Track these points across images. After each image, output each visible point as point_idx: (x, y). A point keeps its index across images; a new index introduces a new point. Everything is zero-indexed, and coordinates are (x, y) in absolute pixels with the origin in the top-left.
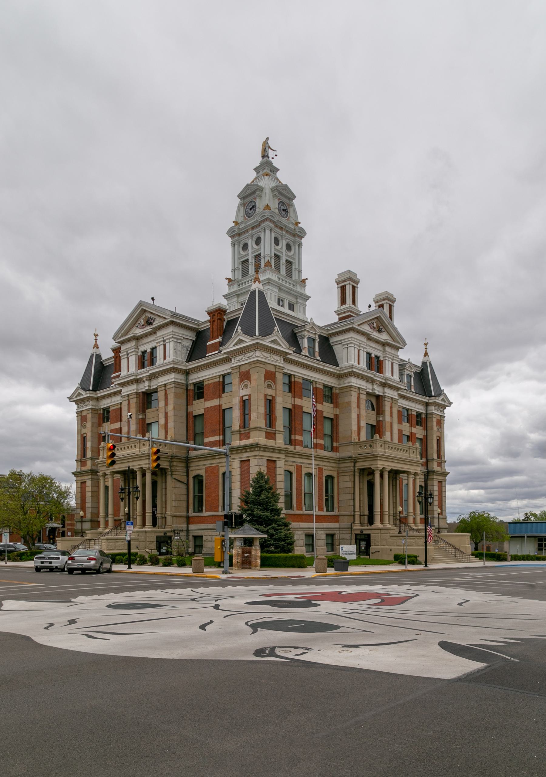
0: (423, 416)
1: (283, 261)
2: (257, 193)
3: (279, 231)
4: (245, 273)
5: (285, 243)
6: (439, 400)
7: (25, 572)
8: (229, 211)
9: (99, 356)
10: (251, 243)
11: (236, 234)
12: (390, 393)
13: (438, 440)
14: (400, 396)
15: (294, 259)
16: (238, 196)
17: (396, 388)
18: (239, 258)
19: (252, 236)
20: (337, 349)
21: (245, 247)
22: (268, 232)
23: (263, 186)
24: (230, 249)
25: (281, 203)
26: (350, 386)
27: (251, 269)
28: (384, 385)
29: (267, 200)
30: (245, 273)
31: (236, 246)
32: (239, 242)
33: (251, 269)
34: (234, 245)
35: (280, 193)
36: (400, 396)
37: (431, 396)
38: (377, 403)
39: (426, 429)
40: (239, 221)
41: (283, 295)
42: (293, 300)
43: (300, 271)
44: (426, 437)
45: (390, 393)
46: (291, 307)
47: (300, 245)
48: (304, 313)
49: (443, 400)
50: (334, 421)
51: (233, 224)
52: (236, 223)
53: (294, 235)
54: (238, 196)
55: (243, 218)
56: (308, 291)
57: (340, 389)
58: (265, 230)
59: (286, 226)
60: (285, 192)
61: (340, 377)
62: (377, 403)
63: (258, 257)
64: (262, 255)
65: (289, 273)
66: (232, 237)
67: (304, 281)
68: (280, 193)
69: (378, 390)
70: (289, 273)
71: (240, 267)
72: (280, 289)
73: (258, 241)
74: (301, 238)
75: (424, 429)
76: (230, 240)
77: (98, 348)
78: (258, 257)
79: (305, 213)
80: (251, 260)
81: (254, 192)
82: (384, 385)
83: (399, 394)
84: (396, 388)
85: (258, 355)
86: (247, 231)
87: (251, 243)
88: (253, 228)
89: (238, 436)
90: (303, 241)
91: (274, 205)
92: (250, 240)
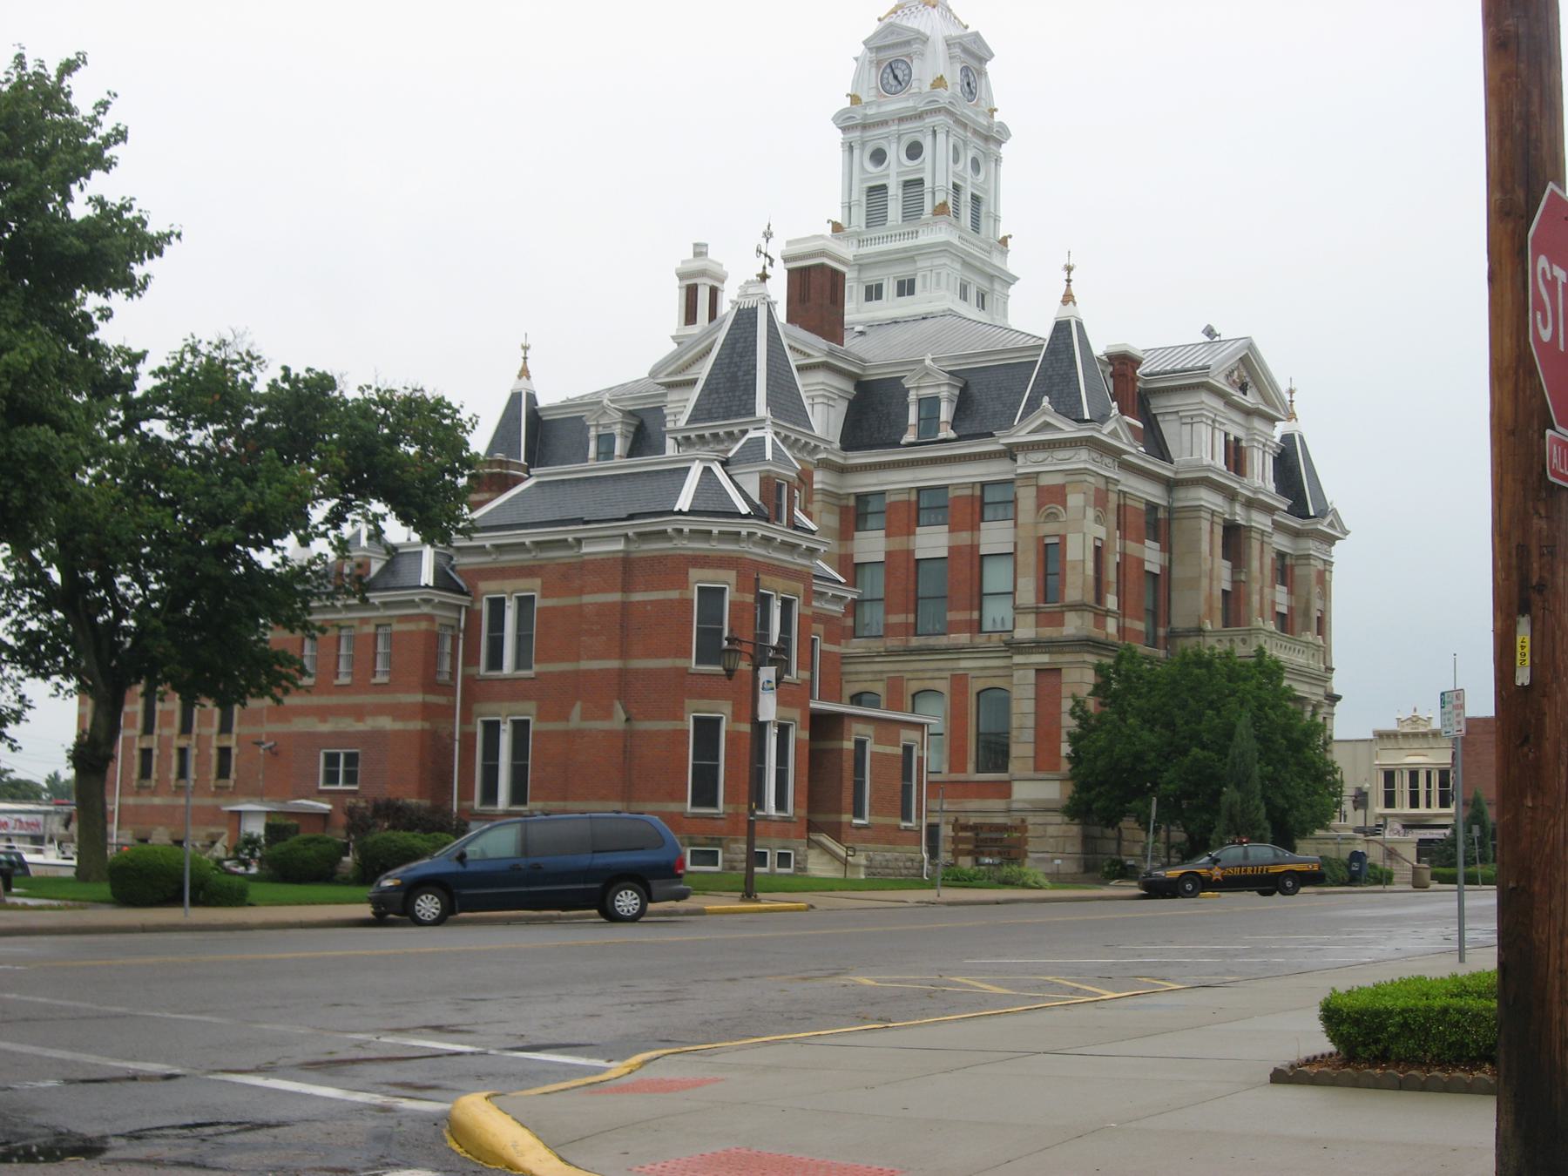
0: (1161, 514)
1: (966, 198)
2: (915, 47)
3: (961, 131)
4: (876, 215)
5: (970, 155)
6: (1323, 527)
7: (701, 912)
8: (837, 74)
9: (532, 398)
10: (896, 153)
11: (855, 125)
12: (1260, 521)
13: (1097, 549)
14: (1278, 526)
15: (986, 192)
16: (865, 43)
17: (1269, 509)
18: (863, 181)
19: (899, 137)
20: (1169, 428)
21: (879, 156)
22: (941, 137)
23: (928, 33)
24: (838, 154)
25: (966, 70)
26: (1199, 508)
27: (894, 209)
28: (1250, 504)
29: (934, 65)
30: (876, 215)
31: (856, 152)
32: (863, 144)
33: (894, 209)
34: (851, 148)
35: (966, 50)
36: (1278, 526)
37: (1307, 516)
38: (1234, 539)
39: (1167, 548)
40: (865, 99)
41: (970, 276)
42: (985, 285)
43: (997, 220)
44: (1167, 570)
45: (1260, 521)
46: (982, 302)
47: (998, 161)
48: (1005, 316)
49: (1331, 525)
50: (1160, 583)
51: (847, 103)
52: (855, 99)
53: (987, 139)
54: (865, 43)
55: (873, 92)
56: (1012, 264)
57: (1299, 557)
58: (934, 132)
59: (974, 122)
60: (974, 48)
61: (1171, 485)
62: (1234, 539)
63: (913, 185)
64: (928, 184)
65: (976, 226)
66: (844, 129)
67: (1004, 241)
68: (966, 50)
69: (1240, 516)
70: (976, 226)
71: (864, 198)
72: (965, 264)
73: (914, 151)
74: (1000, 143)
75: (1162, 550)
76: (839, 135)
77: (528, 377)
78: (913, 185)
79: (1005, 88)
80: (895, 191)
81: (908, 43)
82: (1250, 504)
83: (1274, 522)
84: (1269, 509)
85: (1082, 459)
86: (884, 123)
87: (896, 153)
88: (901, 120)
89: (1031, 618)
90: (1004, 150)
91: (954, 77)
92: (894, 146)
